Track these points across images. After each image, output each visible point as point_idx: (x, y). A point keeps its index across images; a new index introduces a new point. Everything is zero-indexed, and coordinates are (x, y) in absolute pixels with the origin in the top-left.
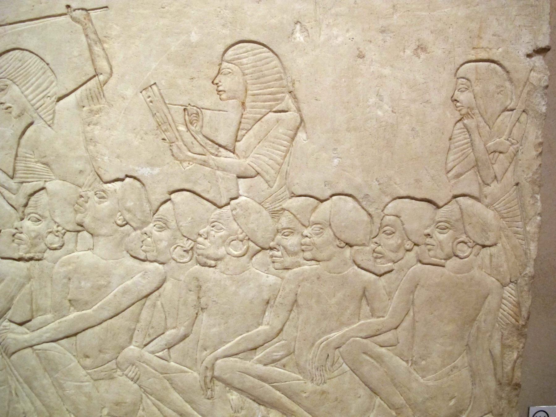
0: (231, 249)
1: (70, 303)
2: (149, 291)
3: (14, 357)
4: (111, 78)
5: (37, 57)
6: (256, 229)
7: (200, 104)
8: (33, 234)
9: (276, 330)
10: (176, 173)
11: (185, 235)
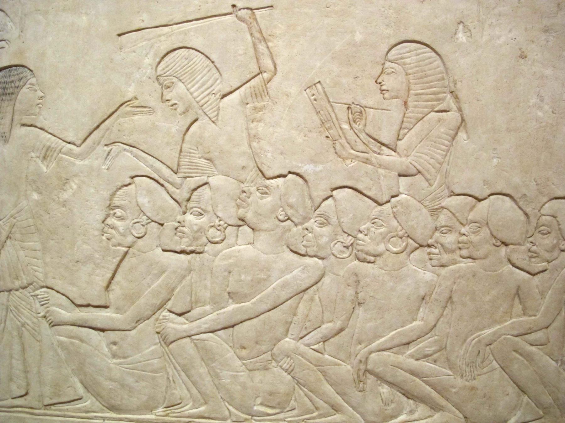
0: (390, 246)
1: (229, 296)
2: (308, 285)
3: (171, 346)
4: (275, 76)
5: (203, 56)
6: (415, 226)
7: (364, 103)
8: (195, 228)
9: (430, 326)
10: (337, 170)
11: (346, 231)
